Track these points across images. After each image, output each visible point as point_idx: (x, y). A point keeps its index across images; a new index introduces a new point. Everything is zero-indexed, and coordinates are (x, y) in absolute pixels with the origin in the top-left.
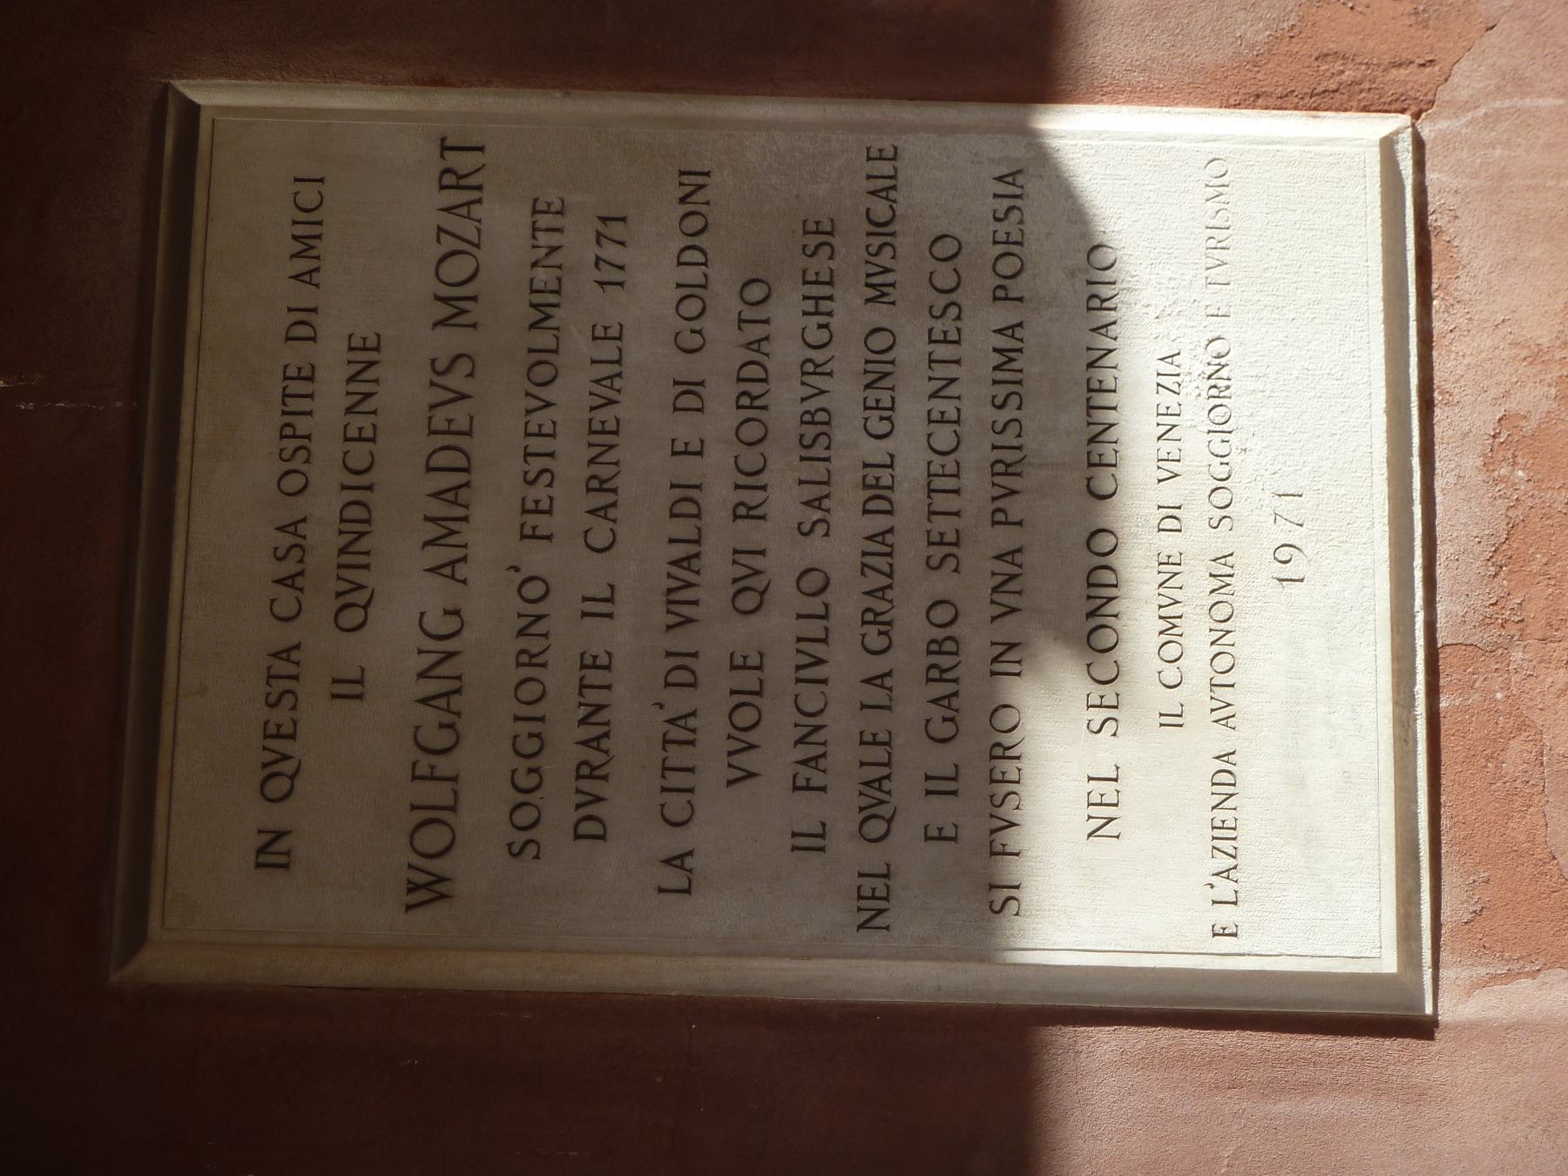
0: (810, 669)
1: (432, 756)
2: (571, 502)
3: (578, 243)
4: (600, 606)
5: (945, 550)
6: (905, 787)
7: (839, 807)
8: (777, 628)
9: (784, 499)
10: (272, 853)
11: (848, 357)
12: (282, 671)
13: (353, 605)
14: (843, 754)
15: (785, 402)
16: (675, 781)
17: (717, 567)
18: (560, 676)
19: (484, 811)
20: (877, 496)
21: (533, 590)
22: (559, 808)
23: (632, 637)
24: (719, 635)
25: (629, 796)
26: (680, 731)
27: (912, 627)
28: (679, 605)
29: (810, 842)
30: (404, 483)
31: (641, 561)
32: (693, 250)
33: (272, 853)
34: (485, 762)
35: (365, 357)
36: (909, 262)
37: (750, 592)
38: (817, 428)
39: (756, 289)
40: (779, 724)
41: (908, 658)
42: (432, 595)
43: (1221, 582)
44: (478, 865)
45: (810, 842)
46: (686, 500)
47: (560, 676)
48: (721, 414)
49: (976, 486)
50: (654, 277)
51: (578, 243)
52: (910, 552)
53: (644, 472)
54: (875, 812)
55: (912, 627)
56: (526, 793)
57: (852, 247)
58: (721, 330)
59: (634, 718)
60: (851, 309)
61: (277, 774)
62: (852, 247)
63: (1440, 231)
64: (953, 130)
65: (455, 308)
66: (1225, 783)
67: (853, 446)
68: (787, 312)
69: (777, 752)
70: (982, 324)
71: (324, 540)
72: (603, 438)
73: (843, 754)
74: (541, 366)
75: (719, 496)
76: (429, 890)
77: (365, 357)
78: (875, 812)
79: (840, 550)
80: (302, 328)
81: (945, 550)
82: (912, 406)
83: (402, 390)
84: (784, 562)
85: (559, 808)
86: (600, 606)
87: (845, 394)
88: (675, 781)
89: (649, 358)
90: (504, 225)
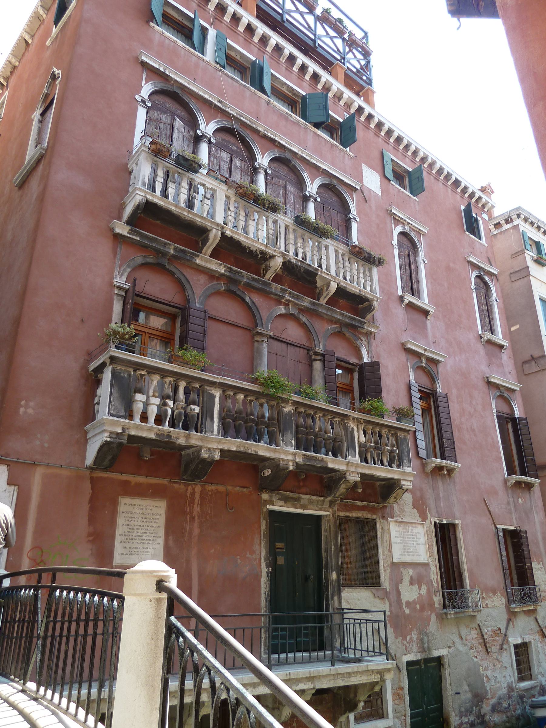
0: (133, 532)
1: (130, 513)
2: (143, 520)
3: (156, 521)
4: (137, 521)
5: (139, 540)
6: (127, 537)
7: (126, 533)
8: (136, 530)
9: (143, 531)
10: (125, 504)
11: (150, 535)
12: (135, 505)
13: (138, 509)
14: (129, 534)
15: (148, 531)
16: (128, 525)
17: (139, 527)
18: (134, 519)
19: (127, 515)
20: (142, 536)
21: (138, 518)
22: (127, 519)
23: (136, 523)
24: (135, 527)
25: (127, 523)
26: (130, 525)
27: (135, 538)
28: (137, 525)
29: (124, 532)
30: (144, 511)
31: (140, 524)
32: (156, 527)
33: (125, 504)
34: (129, 515)
35: (151, 510)
36: (155, 538)
37: (137, 529)
38: (146, 533)
39: (154, 530)
40: (130, 531)
41: (134, 537)
42: (138, 513)
43: (137, 554)
44: (124, 515)
45: (124, 532)
46: (143, 526)
47: (134, 519)
48: (147, 528)
49: (143, 541)
50: (155, 525)
51: (156, 521)
52: (139, 538)
53: (144, 524)
54: (125, 535)
55: (135, 538)
56: (128, 517)
57: (156, 535)
58: (152, 528)
59: (131, 523)
60: (152, 535)
61: (129, 505)
62: (156, 535)
63: (480, 644)
64: (436, 567)
65: (153, 514)
66: (126, 554)
67: (145, 535)
68: (152, 532)
69: (129, 530)
70: (152, 542)
71: (141, 507)
72: (146, 522)
73: (129, 534)
74: (150, 519)
75: (143, 528)
76: (123, 512)
77: (151, 510)
78: (125, 535)
79: (139, 534)
80: (153, 506)
81: (139, 540)
82: (147, 538)
83: (149, 511)
84: (139, 531)
85: (127, 519)
86: (137, 521)
87: (148, 534)
88: (128, 525)
89: (151, 524)
90: (158, 517)
